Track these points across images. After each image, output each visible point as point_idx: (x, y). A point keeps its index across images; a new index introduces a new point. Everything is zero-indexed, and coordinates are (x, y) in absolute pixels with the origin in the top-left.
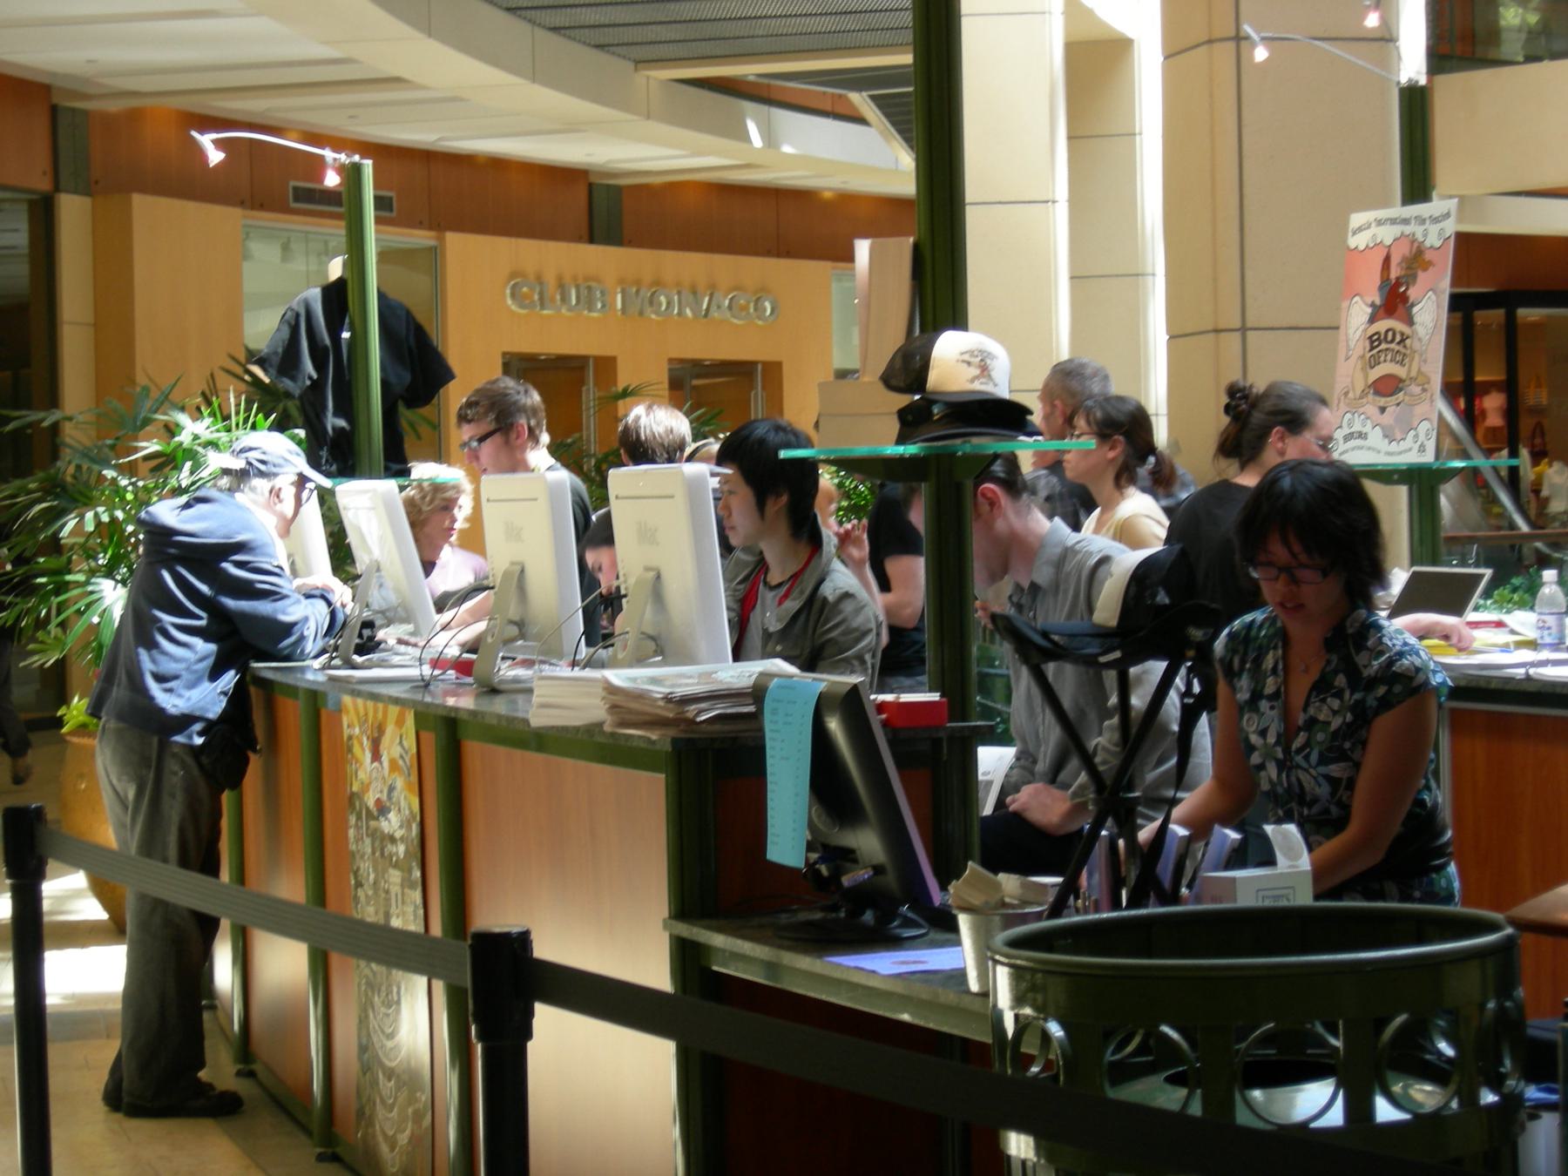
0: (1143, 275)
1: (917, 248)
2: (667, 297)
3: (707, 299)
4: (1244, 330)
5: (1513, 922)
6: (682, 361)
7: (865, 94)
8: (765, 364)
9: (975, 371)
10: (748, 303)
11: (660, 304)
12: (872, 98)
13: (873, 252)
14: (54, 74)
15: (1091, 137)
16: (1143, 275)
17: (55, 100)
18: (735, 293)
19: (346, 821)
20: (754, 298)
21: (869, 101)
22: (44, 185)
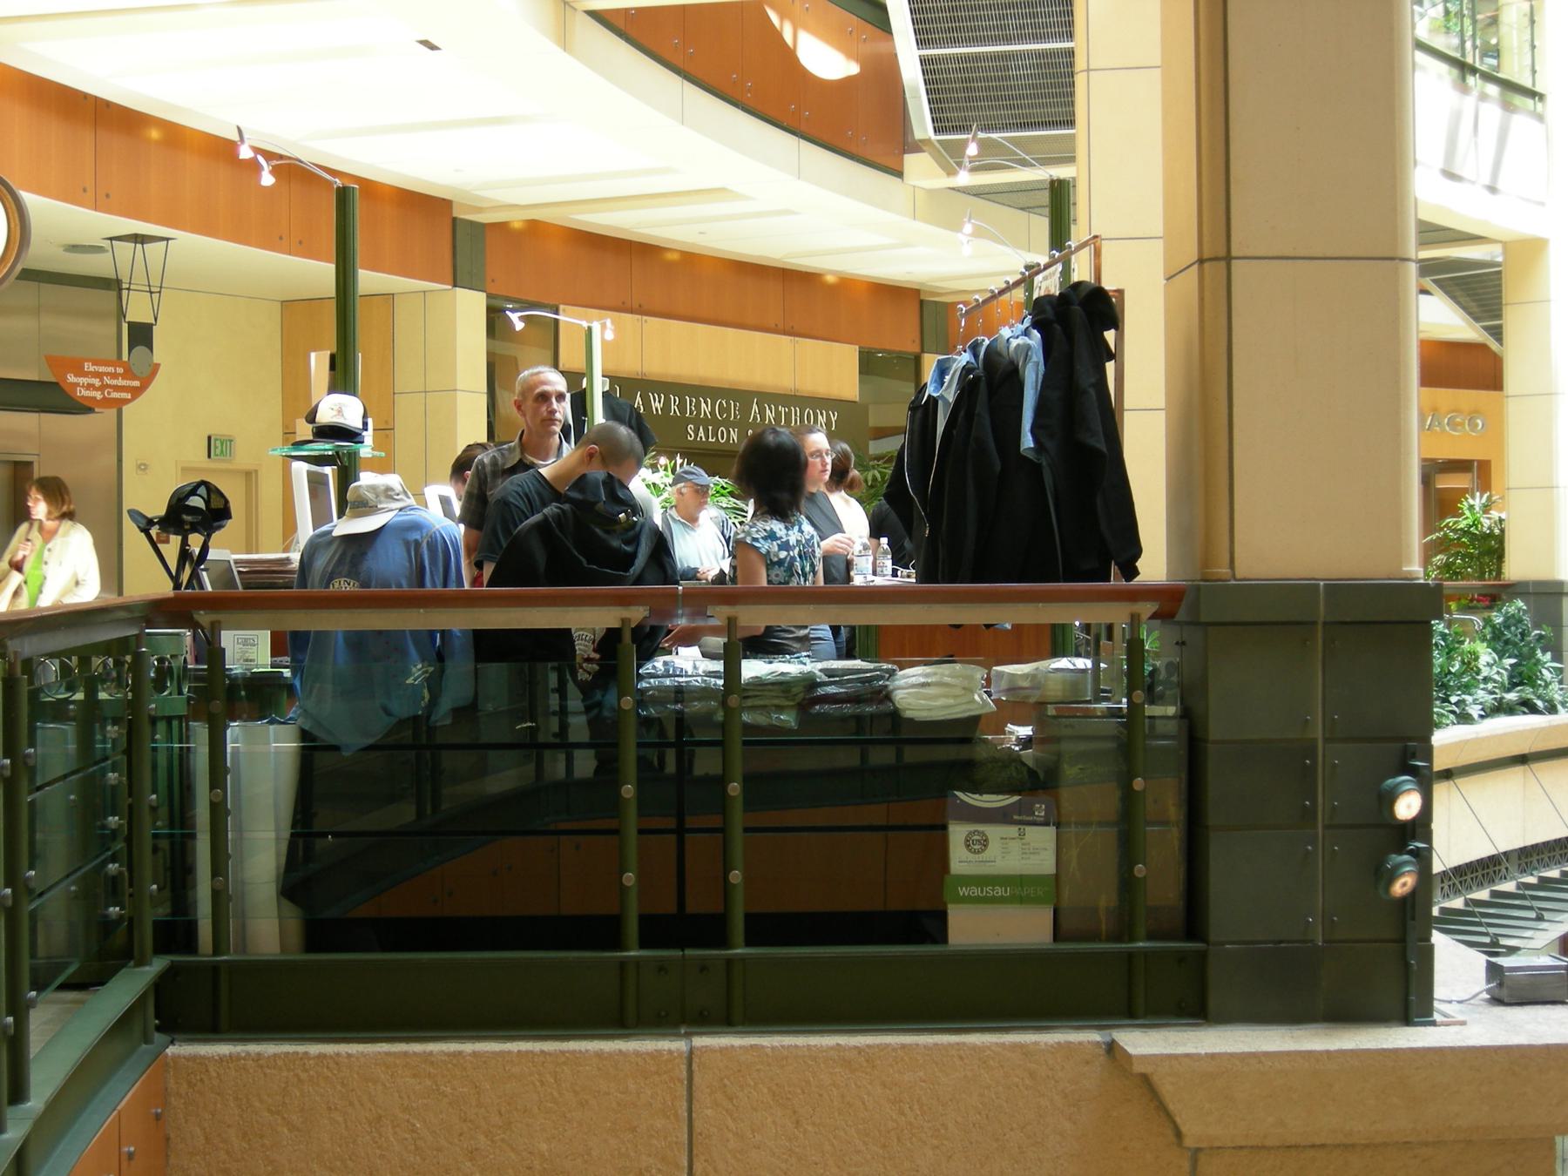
0: (1556, 394)
1: (333, 357)
2: (1482, 421)
3: (1430, 418)
4: (425, 392)
5: (771, 718)
6: (1433, 460)
7: (1428, 279)
8: (1479, 461)
9: (335, 413)
10: (1464, 420)
11: (1477, 425)
12: (1434, 281)
13: (316, 356)
14: (922, 284)
15: (1532, 302)
16: (1556, 394)
17: (922, 297)
18: (1452, 414)
19: (819, 714)
20: (1469, 418)
21: (1431, 282)
22: (916, 349)
